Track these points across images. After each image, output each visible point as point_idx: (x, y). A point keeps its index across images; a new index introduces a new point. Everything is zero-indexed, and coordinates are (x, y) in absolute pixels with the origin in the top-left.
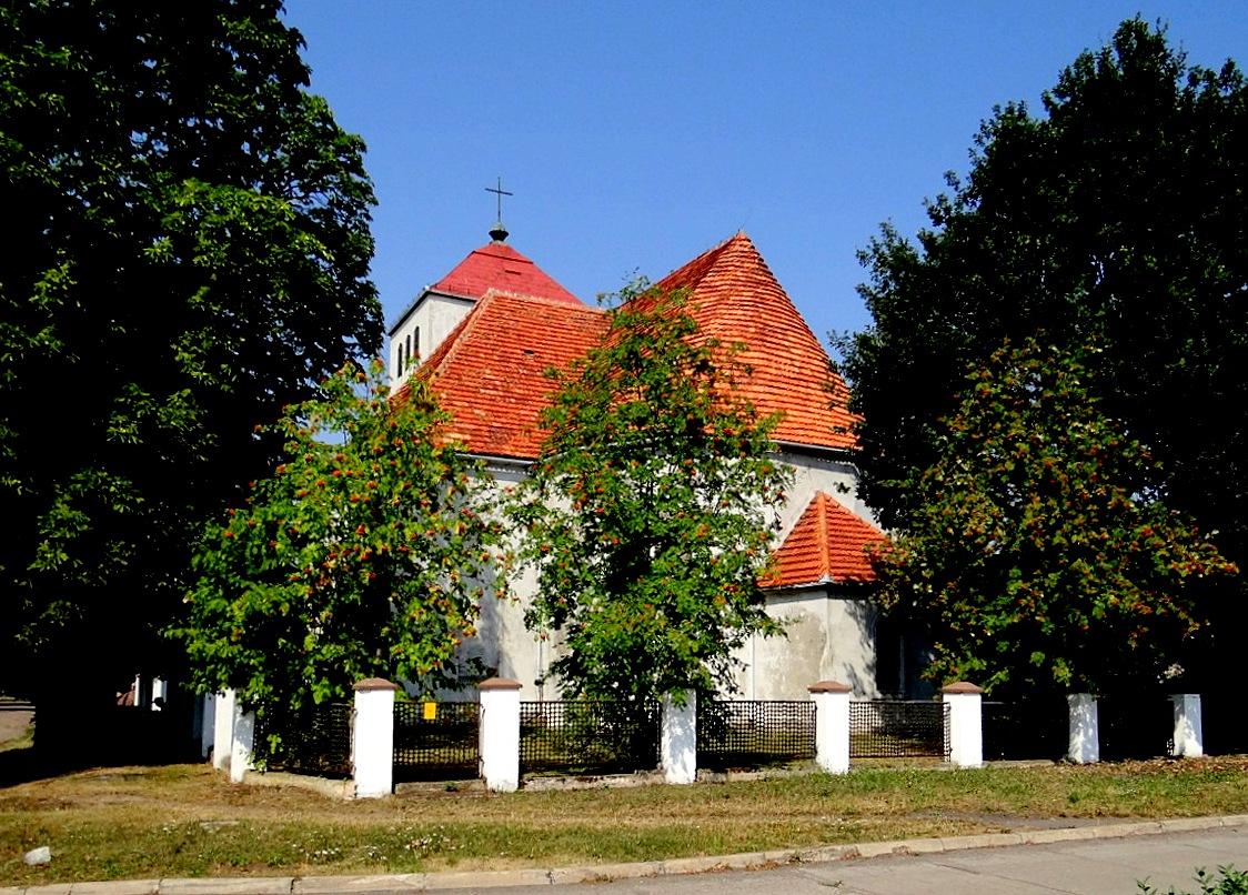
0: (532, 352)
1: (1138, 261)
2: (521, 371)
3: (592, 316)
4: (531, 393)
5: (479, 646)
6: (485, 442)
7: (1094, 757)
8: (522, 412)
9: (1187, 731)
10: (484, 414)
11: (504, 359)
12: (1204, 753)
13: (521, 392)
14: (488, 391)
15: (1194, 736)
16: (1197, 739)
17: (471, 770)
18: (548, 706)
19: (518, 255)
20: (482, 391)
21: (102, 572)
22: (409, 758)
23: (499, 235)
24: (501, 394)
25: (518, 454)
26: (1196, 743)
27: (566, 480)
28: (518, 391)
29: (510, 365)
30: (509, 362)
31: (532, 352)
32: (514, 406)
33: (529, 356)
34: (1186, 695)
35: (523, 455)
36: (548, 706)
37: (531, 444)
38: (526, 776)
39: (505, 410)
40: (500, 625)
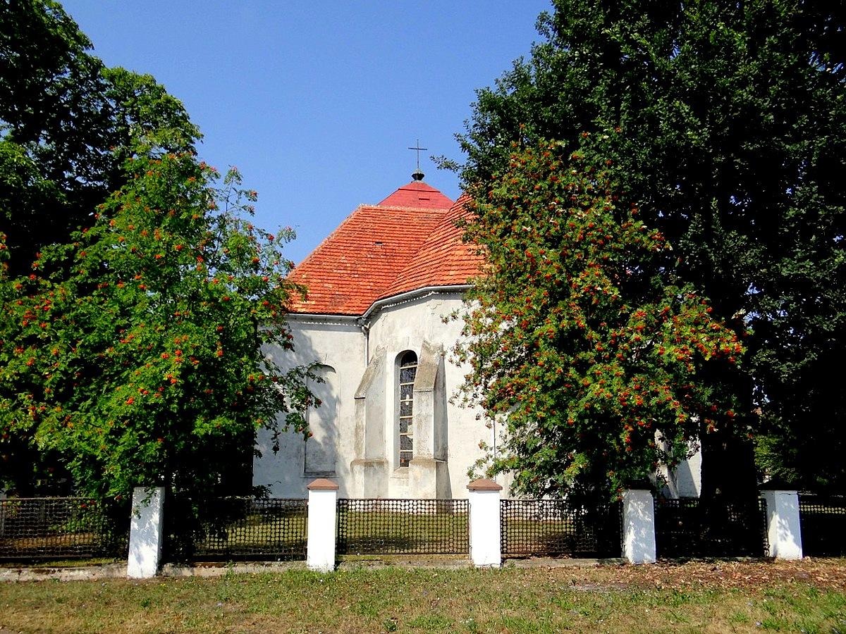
0: (381, 243)
1: (626, 100)
2: (369, 256)
3: (435, 215)
4: (373, 270)
5: (321, 450)
6: (326, 305)
7: (650, 556)
8: (361, 283)
9: (781, 532)
10: (331, 287)
11: (358, 249)
12: (804, 555)
13: (365, 269)
14: (339, 271)
15: (791, 537)
16: (795, 541)
17: (299, 550)
18: (403, 504)
19: (430, 187)
20: (335, 271)
21: (637, 459)
22: (245, 532)
23: (419, 177)
24: (349, 272)
25: (348, 312)
26: (794, 545)
27: (640, 345)
28: (362, 269)
29: (362, 252)
30: (361, 250)
31: (381, 243)
32: (357, 279)
33: (378, 246)
34: (776, 492)
35: (353, 312)
36: (403, 504)
37: (361, 305)
38: (344, 557)
39: (348, 283)
40: (337, 434)
